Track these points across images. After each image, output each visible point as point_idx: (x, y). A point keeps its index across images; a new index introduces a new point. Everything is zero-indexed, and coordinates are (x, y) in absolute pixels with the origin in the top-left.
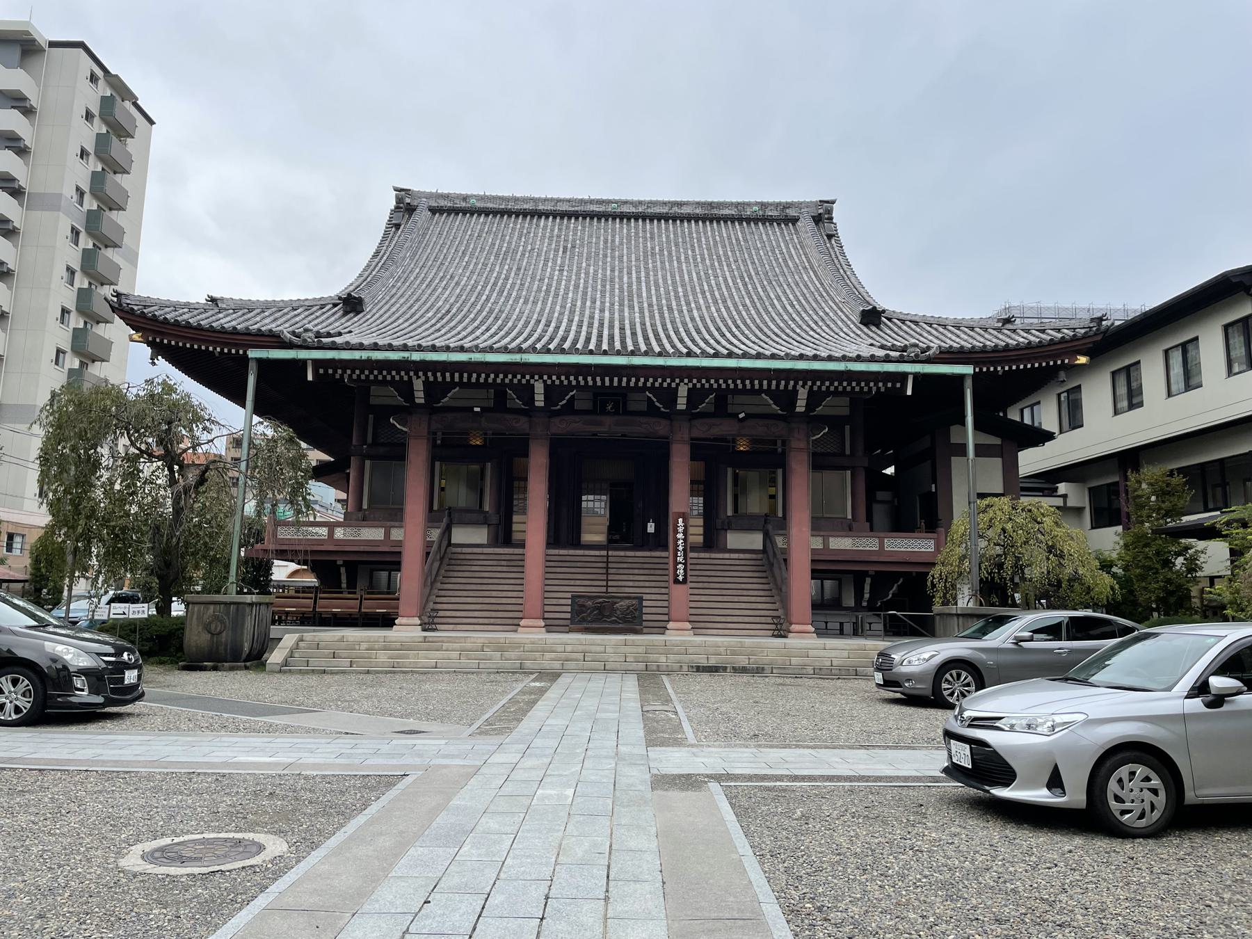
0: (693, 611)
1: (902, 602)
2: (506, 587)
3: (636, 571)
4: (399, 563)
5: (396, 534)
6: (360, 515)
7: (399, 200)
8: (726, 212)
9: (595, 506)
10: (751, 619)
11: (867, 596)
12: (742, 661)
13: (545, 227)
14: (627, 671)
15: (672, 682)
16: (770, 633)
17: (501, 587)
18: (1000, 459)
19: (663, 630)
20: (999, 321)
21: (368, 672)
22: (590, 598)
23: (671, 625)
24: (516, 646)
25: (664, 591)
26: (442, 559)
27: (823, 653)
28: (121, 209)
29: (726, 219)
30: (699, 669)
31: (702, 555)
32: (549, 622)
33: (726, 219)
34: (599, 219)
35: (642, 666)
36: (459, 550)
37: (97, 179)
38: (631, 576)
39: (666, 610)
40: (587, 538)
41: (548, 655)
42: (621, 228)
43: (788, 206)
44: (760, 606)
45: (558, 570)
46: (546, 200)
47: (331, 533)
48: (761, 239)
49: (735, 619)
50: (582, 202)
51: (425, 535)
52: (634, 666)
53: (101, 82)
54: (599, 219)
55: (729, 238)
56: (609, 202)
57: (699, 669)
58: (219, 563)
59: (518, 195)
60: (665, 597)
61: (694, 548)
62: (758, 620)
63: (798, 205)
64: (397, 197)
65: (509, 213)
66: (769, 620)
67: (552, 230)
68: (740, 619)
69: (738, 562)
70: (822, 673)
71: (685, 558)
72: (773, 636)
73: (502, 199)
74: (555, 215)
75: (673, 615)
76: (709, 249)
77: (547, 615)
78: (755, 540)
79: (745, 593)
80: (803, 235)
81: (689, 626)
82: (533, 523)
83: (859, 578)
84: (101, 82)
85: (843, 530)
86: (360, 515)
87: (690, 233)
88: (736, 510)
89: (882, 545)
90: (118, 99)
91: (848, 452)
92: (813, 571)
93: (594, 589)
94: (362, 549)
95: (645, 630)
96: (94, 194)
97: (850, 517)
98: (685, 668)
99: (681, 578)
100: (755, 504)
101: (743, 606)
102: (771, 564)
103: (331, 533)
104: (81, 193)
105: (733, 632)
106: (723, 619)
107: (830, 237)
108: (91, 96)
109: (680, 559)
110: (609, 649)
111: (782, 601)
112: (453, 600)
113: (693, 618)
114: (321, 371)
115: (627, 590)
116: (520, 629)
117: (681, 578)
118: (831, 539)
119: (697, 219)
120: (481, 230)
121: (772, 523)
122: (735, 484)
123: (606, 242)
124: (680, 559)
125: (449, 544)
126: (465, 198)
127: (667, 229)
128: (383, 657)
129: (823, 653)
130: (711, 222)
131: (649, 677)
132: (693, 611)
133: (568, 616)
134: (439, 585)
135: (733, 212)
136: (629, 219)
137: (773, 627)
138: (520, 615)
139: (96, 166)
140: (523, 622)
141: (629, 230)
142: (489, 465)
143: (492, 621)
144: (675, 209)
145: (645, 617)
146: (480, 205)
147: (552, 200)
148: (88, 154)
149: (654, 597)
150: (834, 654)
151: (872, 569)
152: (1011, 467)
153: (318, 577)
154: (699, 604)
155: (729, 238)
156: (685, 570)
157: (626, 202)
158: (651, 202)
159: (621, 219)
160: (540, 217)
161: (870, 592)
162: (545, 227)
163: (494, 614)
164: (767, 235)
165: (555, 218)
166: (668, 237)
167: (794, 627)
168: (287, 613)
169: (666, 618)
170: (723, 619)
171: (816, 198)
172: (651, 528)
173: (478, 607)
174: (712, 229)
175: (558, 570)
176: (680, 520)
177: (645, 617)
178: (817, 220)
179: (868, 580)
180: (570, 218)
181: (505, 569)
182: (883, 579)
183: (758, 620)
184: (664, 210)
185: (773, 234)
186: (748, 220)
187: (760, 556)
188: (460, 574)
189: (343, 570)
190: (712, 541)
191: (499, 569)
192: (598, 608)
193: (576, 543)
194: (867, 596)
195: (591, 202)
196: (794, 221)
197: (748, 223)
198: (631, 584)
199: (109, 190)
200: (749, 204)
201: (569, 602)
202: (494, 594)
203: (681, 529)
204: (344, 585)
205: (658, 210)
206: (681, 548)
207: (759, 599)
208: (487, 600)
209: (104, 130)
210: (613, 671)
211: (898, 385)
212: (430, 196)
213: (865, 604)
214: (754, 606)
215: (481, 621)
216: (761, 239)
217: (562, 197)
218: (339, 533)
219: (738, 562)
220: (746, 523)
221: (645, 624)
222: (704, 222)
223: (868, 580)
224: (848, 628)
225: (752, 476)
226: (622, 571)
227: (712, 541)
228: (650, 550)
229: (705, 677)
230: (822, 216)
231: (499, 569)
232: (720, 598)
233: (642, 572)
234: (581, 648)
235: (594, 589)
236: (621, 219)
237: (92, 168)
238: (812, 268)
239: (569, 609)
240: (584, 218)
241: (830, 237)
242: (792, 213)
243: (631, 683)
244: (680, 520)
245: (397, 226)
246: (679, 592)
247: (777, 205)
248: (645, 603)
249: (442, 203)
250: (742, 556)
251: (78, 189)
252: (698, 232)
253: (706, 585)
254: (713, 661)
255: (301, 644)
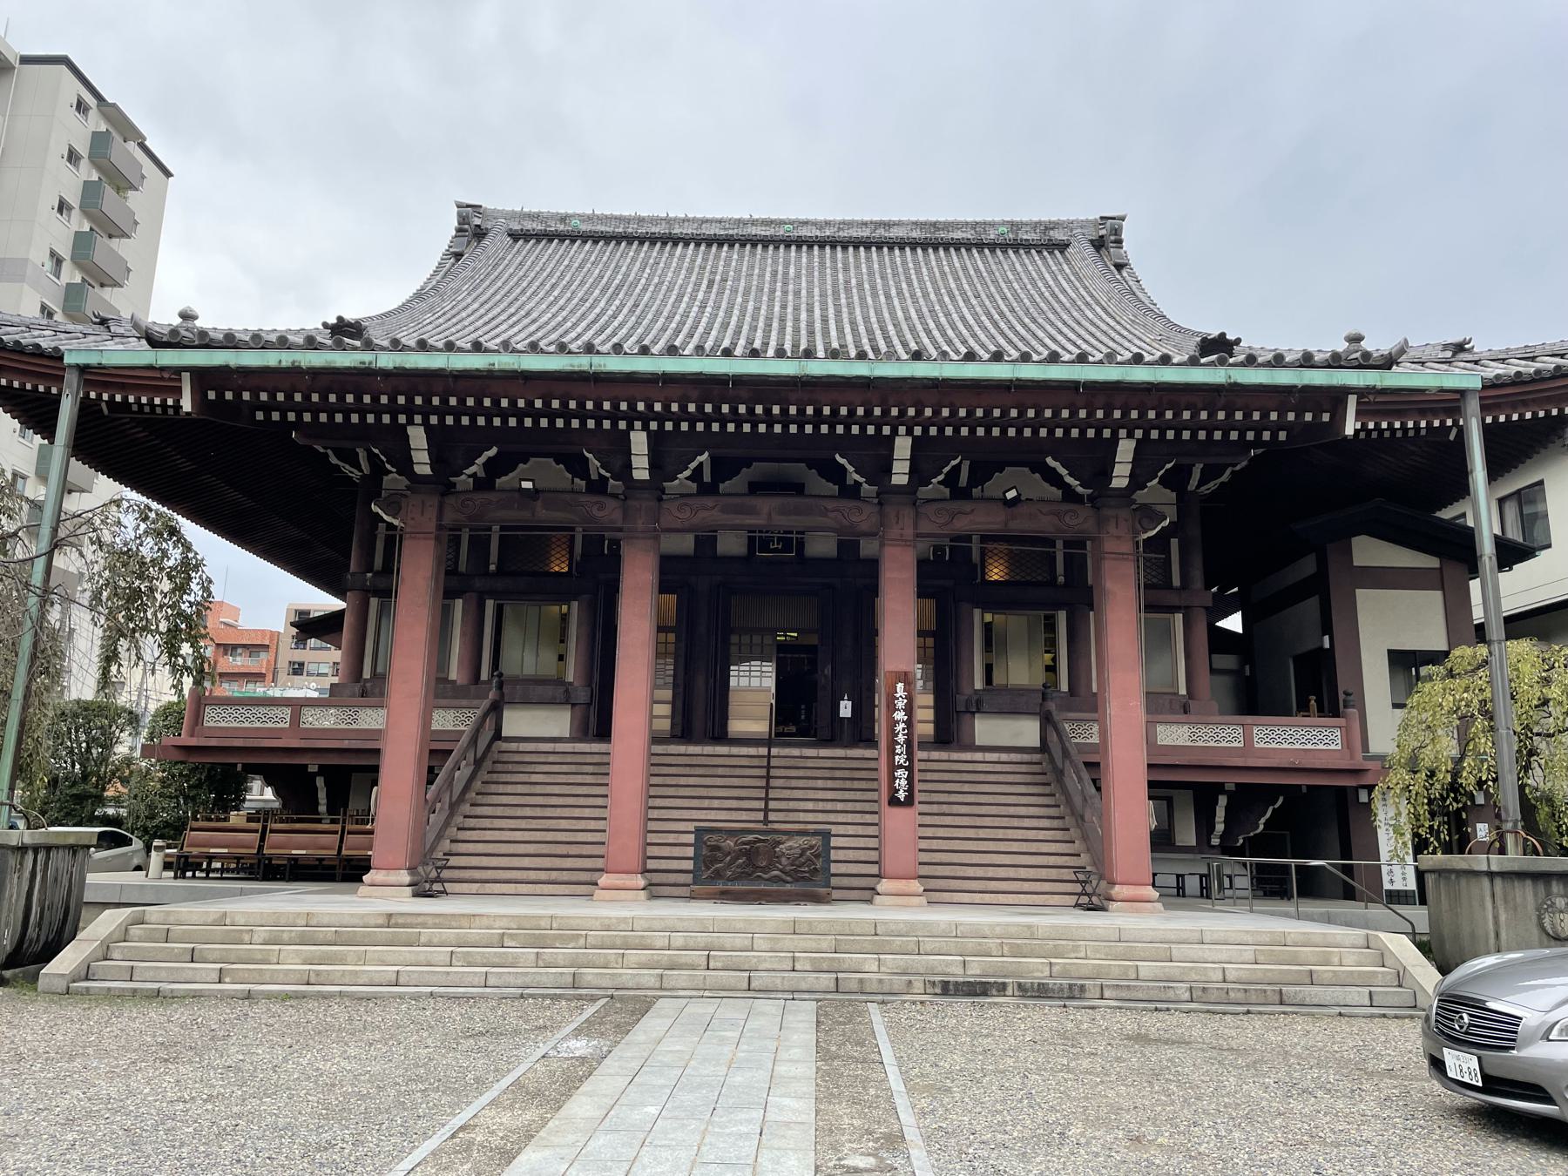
0: (925, 857)
1: (1289, 839)
2: (587, 812)
3: (820, 783)
4: (375, 769)
5: (370, 719)
6: (357, 688)
7: (463, 220)
8: (958, 235)
9: (754, 684)
10: (1031, 873)
11: (1220, 827)
12: (1036, 968)
13: (683, 257)
14: (794, 993)
15: (893, 1028)
16: (1072, 900)
17: (577, 812)
18: (1438, 594)
19: (868, 894)
20: (1445, 347)
21: (249, 996)
22: (732, 833)
23: (884, 885)
24: (570, 934)
25: (868, 818)
26: (478, 763)
27: (1195, 951)
28: (116, 284)
29: (958, 245)
30: (948, 989)
31: (935, 755)
32: (657, 878)
33: (958, 245)
34: (765, 247)
35: (826, 980)
36: (513, 746)
37: (82, 242)
38: (812, 794)
39: (873, 855)
40: (737, 726)
41: (633, 956)
42: (799, 259)
43: (1050, 226)
44: (1045, 847)
45: (683, 781)
46: (686, 220)
47: (296, 719)
48: (1013, 270)
49: (1002, 872)
50: (739, 222)
51: (426, 720)
52: (811, 980)
53: (93, 113)
54: (765, 247)
55: (965, 269)
56: (782, 223)
57: (948, 989)
58: (1495, 815)
59: (644, 214)
60: (872, 830)
61: (924, 745)
62: (1043, 873)
63: (1068, 225)
64: (459, 215)
65: (630, 239)
66: (1067, 874)
67: (693, 261)
68: (1011, 873)
69: (998, 768)
70: (1218, 999)
71: (910, 758)
72: (1077, 905)
73: (620, 219)
74: (698, 241)
75: (889, 865)
76: (934, 282)
77: (651, 864)
78: (1027, 731)
79: (1015, 822)
80: (1077, 264)
81: (916, 886)
82: (640, 692)
83: (1204, 797)
84: (93, 113)
85: (1173, 712)
86: (357, 688)
87: (904, 263)
88: (989, 679)
89: (1248, 739)
90: (118, 138)
91: (1176, 582)
92: (1152, 785)
93: (744, 816)
94: (346, 744)
95: (836, 894)
96: (77, 261)
97: (1183, 691)
98: (918, 986)
99: (902, 795)
100: (1021, 671)
101: (1015, 847)
102: (1065, 776)
103: (296, 719)
104: (58, 261)
105: (1001, 898)
106: (980, 872)
107: (1119, 267)
108: (80, 131)
109: (900, 759)
110: (760, 943)
111: (1085, 838)
112: (489, 835)
113: (925, 870)
114: (212, 395)
115: (802, 817)
116: (598, 893)
117: (902, 795)
118: (1160, 728)
119: (914, 245)
120: (584, 261)
121: (1065, 699)
122: (988, 644)
123: (774, 274)
124: (900, 759)
125: (497, 735)
126: (564, 219)
127: (869, 259)
128: (292, 961)
129: (1195, 951)
130: (936, 249)
131: (841, 1003)
132: (925, 857)
133: (689, 865)
134: (466, 808)
135: (969, 235)
136: (810, 247)
137: (1078, 888)
138: (599, 863)
139: (81, 224)
140: (604, 880)
141: (810, 261)
142: (575, 604)
143: (554, 875)
144: (881, 232)
145: (834, 868)
146: (584, 227)
147: (694, 220)
148: (70, 208)
149: (851, 830)
150: (1224, 952)
151: (1230, 780)
152: (1457, 607)
153: (277, 793)
154: (935, 844)
155: (965, 269)
156: (910, 779)
157: (806, 223)
158: (844, 223)
159: (799, 247)
160: (675, 244)
161: (1225, 822)
162: (683, 257)
163: (558, 863)
164: (1023, 265)
165: (698, 245)
166: (870, 268)
167: (1117, 890)
168: (211, 858)
169: (874, 869)
170: (980, 872)
171: (1094, 215)
172: (846, 709)
173: (531, 849)
174: (938, 259)
175: (683, 781)
176: (900, 686)
177: (834, 868)
178: (1099, 244)
179: (1223, 801)
180: (721, 245)
181: (589, 779)
182: (1248, 798)
183: (1043, 873)
184: (865, 233)
185: (1033, 263)
186: (993, 247)
187: (1036, 757)
188: (509, 789)
189: (320, 782)
190: (948, 733)
191: (579, 779)
192: (747, 854)
193: (720, 735)
194: (1220, 827)
195: (754, 222)
196: (1063, 247)
197: (993, 251)
198: (810, 806)
199: (99, 257)
200: (993, 224)
201: (691, 838)
202: (564, 824)
203: (900, 704)
204: (322, 808)
205: (855, 233)
206: (901, 738)
207: (1042, 835)
208: (550, 836)
209: (95, 177)
210: (767, 992)
211: (1326, 417)
212: (512, 215)
213: (1215, 841)
214: (1034, 847)
215: (533, 875)
216: (1013, 270)
217: (709, 216)
218: (317, 720)
219: (998, 768)
220: (1010, 704)
221: (834, 881)
222: (924, 250)
223: (1223, 801)
224: (1192, 884)
225: (1013, 623)
226: (794, 783)
227: (948, 733)
228: (846, 747)
229: (962, 1004)
230: (1106, 239)
231: (579, 779)
232: (971, 833)
233: (830, 784)
234: (702, 939)
235: (744, 816)
236: (799, 247)
237: (75, 227)
238: (1098, 303)
239: (690, 852)
240: (743, 245)
241: (1119, 267)
242: (1058, 235)
243: (805, 1012)
244: (900, 686)
245: (458, 256)
246: (899, 822)
247: (1035, 225)
248: (834, 842)
249: (529, 225)
250: (1004, 757)
251: (53, 254)
252: (916, 263)
253: (945, 809)
254: (976, 970)
255: (135, 931)
